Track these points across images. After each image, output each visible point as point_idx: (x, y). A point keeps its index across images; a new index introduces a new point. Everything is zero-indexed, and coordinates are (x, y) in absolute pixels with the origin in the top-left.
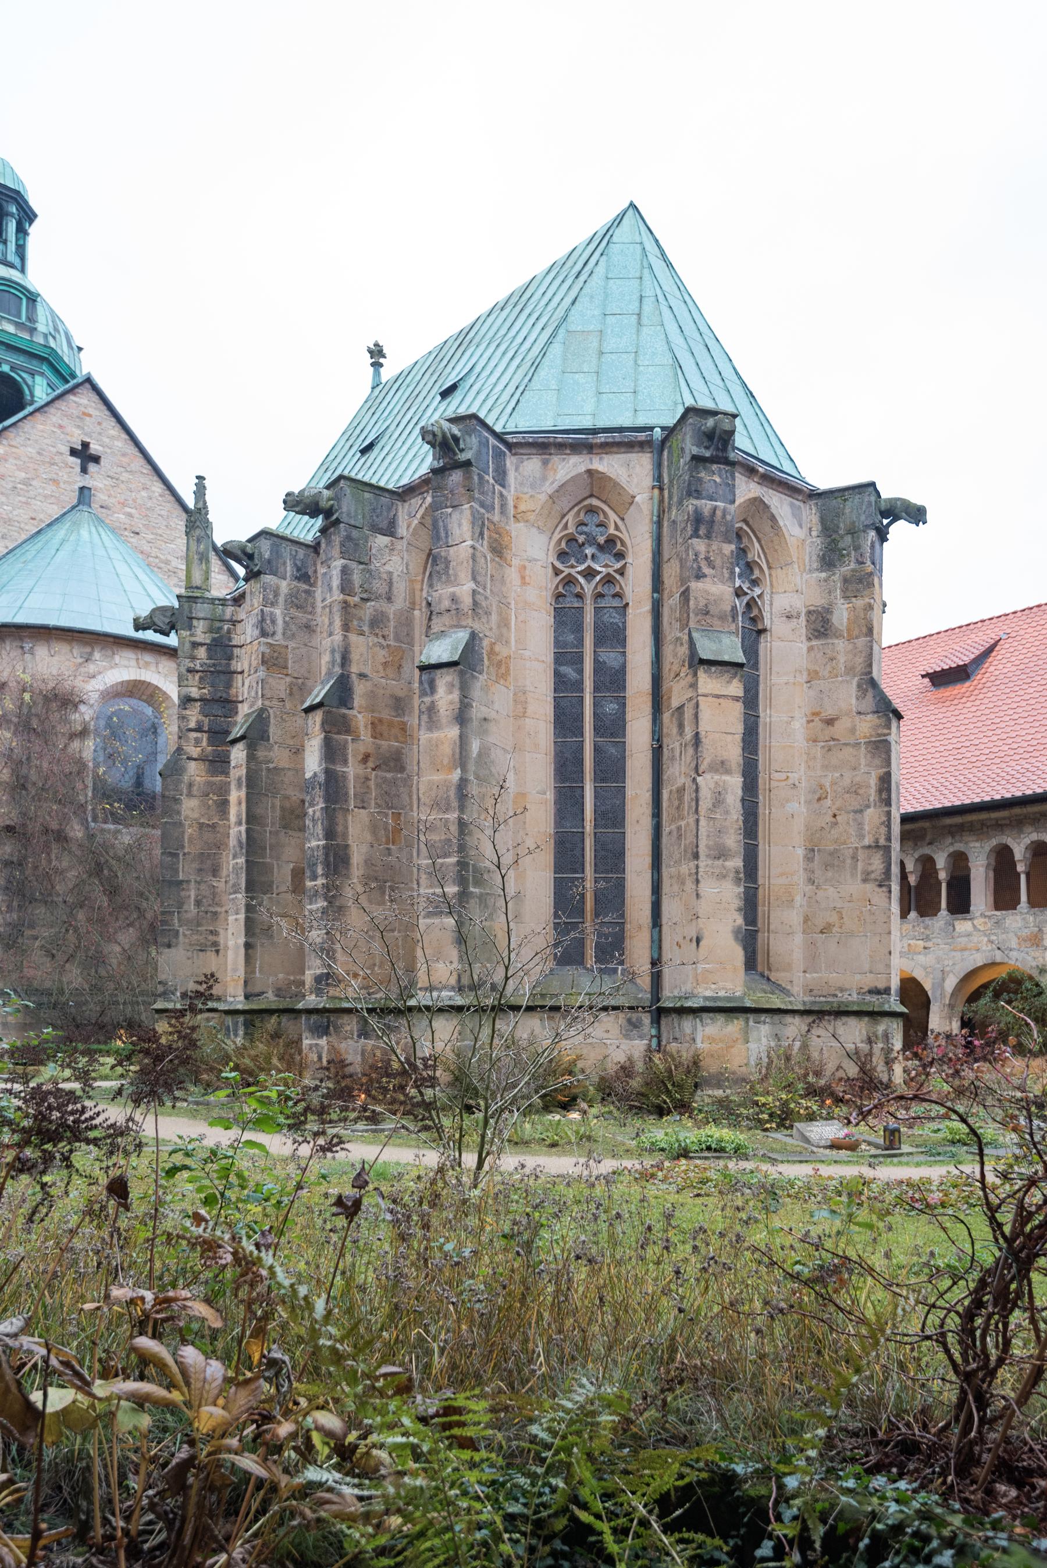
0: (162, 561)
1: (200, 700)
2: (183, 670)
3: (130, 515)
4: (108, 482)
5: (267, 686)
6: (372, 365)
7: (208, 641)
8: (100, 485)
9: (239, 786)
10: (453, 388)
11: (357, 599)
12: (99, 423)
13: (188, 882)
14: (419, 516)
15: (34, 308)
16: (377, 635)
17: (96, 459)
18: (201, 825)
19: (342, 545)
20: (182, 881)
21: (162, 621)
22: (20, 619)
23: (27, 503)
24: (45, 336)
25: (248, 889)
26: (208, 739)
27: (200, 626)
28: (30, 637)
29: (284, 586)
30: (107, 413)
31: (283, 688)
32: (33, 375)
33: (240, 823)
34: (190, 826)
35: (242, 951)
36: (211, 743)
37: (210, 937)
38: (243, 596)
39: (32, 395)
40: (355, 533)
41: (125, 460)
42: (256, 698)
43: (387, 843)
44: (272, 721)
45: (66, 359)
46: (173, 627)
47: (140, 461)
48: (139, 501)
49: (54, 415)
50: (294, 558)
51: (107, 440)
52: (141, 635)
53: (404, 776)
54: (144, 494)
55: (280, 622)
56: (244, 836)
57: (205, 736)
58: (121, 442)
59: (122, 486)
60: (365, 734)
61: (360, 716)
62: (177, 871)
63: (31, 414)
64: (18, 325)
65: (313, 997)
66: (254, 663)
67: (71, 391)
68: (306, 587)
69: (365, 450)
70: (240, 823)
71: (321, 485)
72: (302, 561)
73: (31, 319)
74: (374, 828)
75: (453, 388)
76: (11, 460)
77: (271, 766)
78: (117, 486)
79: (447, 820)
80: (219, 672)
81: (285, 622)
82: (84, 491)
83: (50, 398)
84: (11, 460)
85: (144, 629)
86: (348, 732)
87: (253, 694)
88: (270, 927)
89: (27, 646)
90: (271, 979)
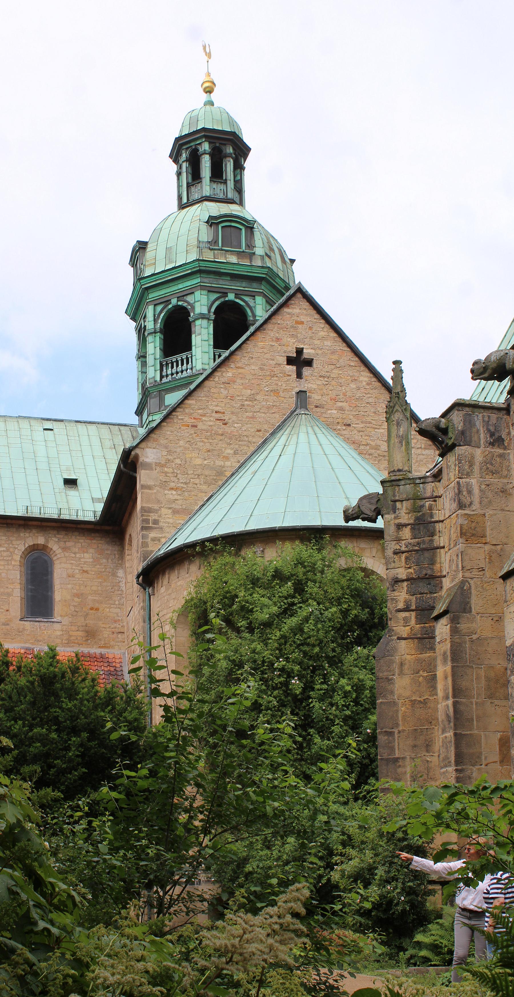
0: (372, 448)
1: (407, 580)
3: (341, 409)
4: (322, 381)
5: (466, 558)
7: (412, 521)
8: (314, 386)
12: (311, 328)
13: (404, 758)
15: (252, 233)
18: (413, 702)
21: (368, 509)
22: (253, 526)
23: (253, 417)
24: (262, 257)
25: (457, 763)
26: (416, 618)
27: (403, 508)
28: (262, 542)
29: (479, 454)
30: (317, 316)
33: (447, 698)
34: (403, 705)
36: (419, 620)
38: (440, 471)
39: (254, 316)
42: (457, 571)
44: (473, 591)
47: (349, 354)
48: (348, 394)
49: (272, 331)
50: (487, 423)
51: (317, 342)
52: (352, 524)
54: (353, 386)
55: (476, 491)
57: (413, 614)
59: (333, 383)
62: (392, 749)
63: (253, 334)
64: (240, 254)
66: (454, 536)
67: (285, 304)
68: (501, 451)
71: (509, 347)
72: (495, 426)
73: (250, 245)
76: (239, 381)
77: (474, 637)
81: (481, 490)
82: (301, 394)
83: (270, 313)
84: (239, 381)
85: (353, 519)
87: (454, 567)
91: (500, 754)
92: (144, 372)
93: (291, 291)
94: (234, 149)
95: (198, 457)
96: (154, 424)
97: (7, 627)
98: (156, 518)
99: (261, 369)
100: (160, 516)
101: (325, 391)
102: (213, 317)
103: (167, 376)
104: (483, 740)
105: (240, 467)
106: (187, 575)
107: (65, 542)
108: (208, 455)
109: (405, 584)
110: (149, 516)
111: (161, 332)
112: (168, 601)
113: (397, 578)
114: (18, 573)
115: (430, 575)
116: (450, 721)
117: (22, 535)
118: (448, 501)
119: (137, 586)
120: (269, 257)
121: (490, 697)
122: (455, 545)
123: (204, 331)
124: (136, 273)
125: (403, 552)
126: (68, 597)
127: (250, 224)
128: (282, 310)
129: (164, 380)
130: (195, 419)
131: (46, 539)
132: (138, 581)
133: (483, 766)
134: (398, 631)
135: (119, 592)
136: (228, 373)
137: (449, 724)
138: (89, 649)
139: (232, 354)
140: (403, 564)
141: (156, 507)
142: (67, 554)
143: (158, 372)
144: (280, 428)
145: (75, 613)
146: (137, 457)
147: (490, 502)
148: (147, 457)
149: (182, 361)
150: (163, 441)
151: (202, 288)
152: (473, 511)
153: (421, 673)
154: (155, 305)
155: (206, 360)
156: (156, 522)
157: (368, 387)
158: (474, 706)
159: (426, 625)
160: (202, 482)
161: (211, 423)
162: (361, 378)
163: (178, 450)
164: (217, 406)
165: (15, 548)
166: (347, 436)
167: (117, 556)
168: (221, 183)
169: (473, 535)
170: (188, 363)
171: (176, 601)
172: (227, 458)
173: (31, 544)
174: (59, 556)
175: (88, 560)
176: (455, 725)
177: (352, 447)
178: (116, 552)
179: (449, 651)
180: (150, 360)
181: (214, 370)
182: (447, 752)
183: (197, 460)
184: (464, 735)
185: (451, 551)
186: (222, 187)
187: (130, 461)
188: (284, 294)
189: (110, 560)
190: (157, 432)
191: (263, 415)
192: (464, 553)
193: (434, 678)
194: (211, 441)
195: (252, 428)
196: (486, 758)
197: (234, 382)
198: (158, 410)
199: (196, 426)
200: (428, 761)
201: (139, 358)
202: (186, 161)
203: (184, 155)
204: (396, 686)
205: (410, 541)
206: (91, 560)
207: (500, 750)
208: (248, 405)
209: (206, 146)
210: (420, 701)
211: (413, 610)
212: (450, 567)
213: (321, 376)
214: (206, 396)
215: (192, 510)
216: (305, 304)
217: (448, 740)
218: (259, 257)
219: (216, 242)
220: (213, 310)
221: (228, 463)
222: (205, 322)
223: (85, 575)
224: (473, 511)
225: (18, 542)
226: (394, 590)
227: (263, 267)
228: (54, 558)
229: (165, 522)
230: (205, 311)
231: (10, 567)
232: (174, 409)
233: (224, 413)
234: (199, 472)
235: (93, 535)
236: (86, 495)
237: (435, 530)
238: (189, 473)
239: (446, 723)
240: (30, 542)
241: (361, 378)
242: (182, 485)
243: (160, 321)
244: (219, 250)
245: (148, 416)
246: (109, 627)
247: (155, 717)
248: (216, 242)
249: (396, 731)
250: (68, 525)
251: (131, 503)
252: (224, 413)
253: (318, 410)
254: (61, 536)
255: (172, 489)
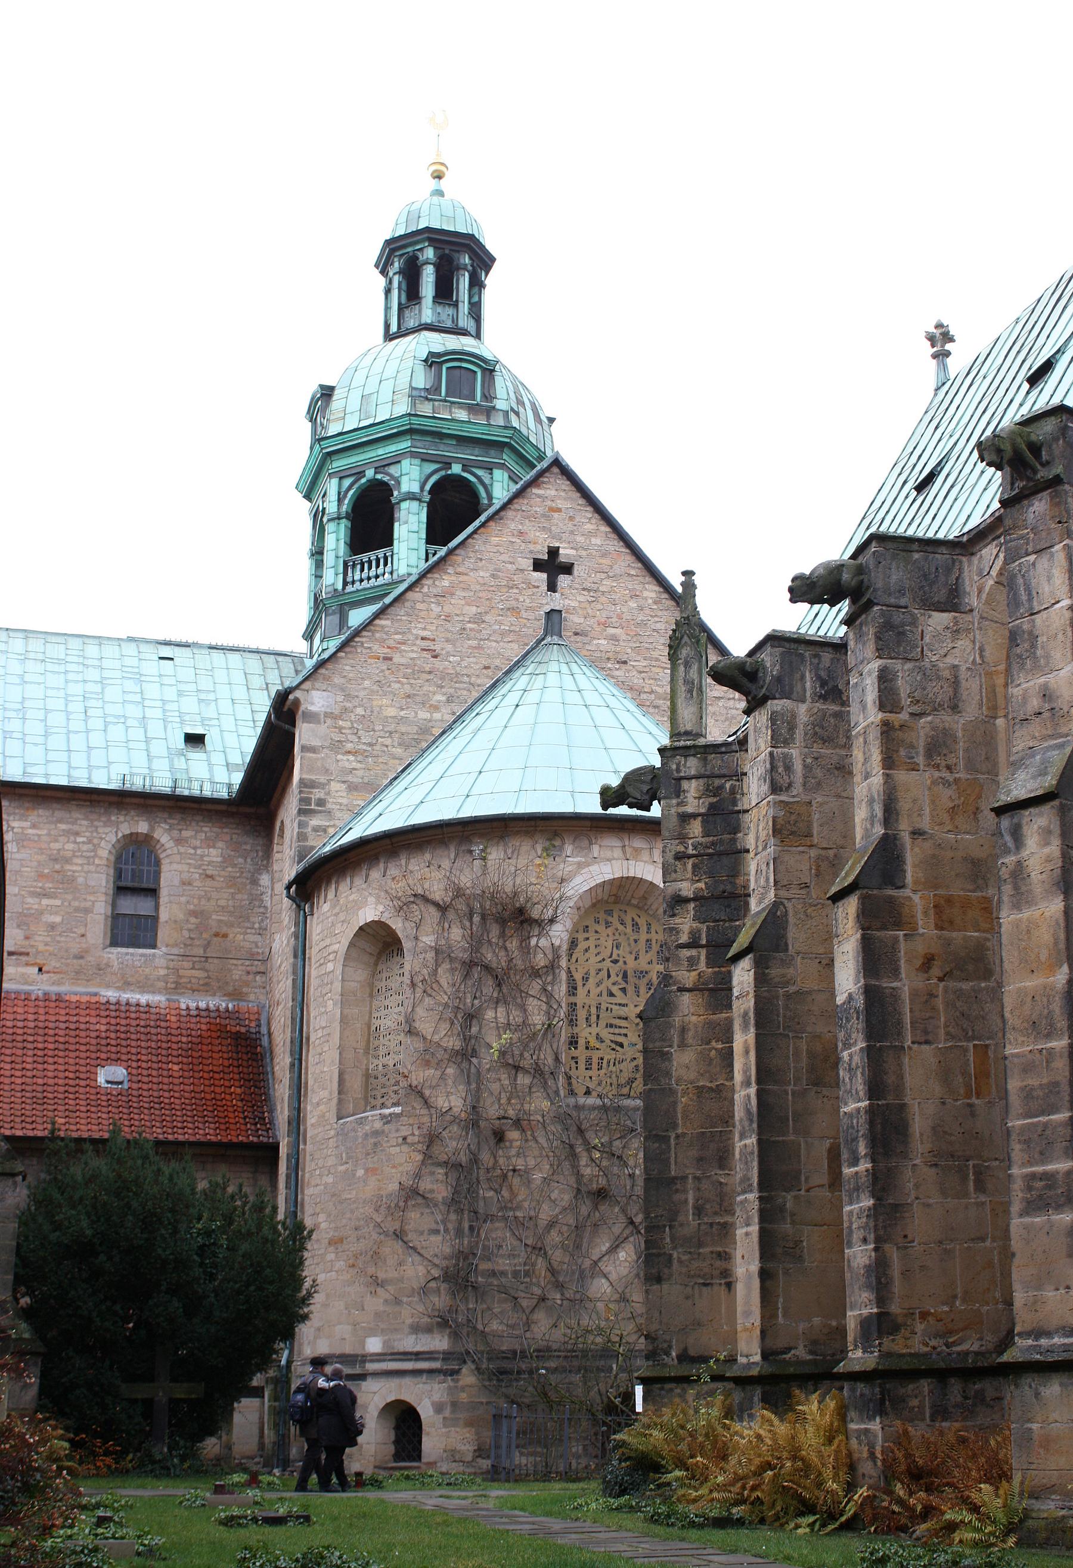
1: (694, 899)
2: (670, 856)
3: (614, 638)
5: (782, 868)
6: (935, 356)
7: (702, 810)
9: (745, 1027)
10: (1047, 367)
11: (904, 716)
12: (571, 518)
14: (994, 573)
16: (937, 767)
17: (568, 569)
18: (700, 1090)
19: (878, 638)
20: (676, 1178)
22: (469, 811)
24: (506, 413)
25: (763, 1185)
26: (707, 958)
27: (692, 788)
28: (482, 836)
29: (803, 711)
30: (582, 501)
31: (805, 867)
32: (490, 470)
34: (685, 1093)
35: (756, 1283)
37: (718, 1263)
39: (490, 497)
40: (897, 618)
41: (605, 561)
43: (968, 1096)
44: (791, 919)
45: (533, 440)
46: (653, 798)
49: (513, 521)
51: (580, 539)
53: (992, 984)
54: (633, 604)
55: (798, 767)
56: (754, 1102)
57: (703, 952)
58: (600, 538)
59: (603, 599)
60: (925, 927)
61: (916, 898)
63: (483, 525)
64: (472, 409)
65: (859, 1353)
66: (763, 835)
67: (534, 482)
69: (921, 487)
70: (747, 1083)
72: (829, 670)
73: (489, 396)
74: (945, 1075)
75: (1047, 367)
76: (460, 593)
77: (792, 989)
78: (596, 601)
79: (1051, 1051)
80: (720, 854)
81: (805, 766)
82: (553, 617)
84: (460, 593)
85: (615, 805)
86: (898, 925)
87: (762, 882)
88: (798, 1243)
89: (477, 849)
90: (802, 1326)
91: (829, 1174)
92: (318, 576)
93: (545, 464)
94: (470, 258)
95: (392, 706)
96: (326, 655)
97: (81, 961)
98: (322, 795)
99: (493, 576)
100: (328, 793)
101: (590, 611)
102: (427, 498)
103: (353, 582)
104: (803, 1152)
105: (454, 722)
106: (364, 886)
107: (180, 830)
108: (407, 703)
109: (692, 905)
110: (311, 793)
111: (347, 517)
112: (333, 925)
113: (679, 896)
114: (104, 877)
115: (730, 893)
116: (751, 1121)
117: (113, 818)
118: (755, 782)
119: (287, 902)
120: (517, 414)
121: (816, 1084)
122: (765, 848)
123: (413, 519)
124: (314, 431)
125: (689, 857)
126: (181, 916)
127: (490, 365)
128: (529, 490)
129: (349, 588)
130: (389, 647)
131: (150, 825)
132: (289, 892)
133: (802, 1192)
134: (680, 978)
135: (262, 910)
136: (444, 581)
137: (750, 1125)
138: (138, 996)
139: (451, 552)
140: (689, 875)
141: (322, 779)
142: (182, 850)
143: (341, 577)
144: (518, 664)
145: (189, 942)
146: (297, 703)
147: (819, 784)
148: (313, 704)
149: (378, 560)
150: (337, 680)
151: (413, 455)
152: (794, 796)
153: (714, 1044)
154: (341, 478)
155: (414, 562)
156: (321, 802)
157: (655, 607)
158: (790, 1097)
159: (723, 969)
160: (396, 744)
161: (414, 655)
162: (646, 594)
163: (362, 694)
164: (424, 629)
165: (102, 839)
166: (620, 679)
167: (260, 854)
168: (450, 305)
169: (793, 833)
170: (386, 564)
171: (345, 925)
172: (436, 708)
173: (128, 832)
174: (169, 852)
175: (215, 859)
176: (759, 1126)
177: (629, 695)
178: (259, 848)
179: (752, 1010)
180: (329, 558)
181: (423, 575)
182: (748, 1170)
183: (389, 709)
184: (774, 1142)
185: (758, 857)
186: (450, 311)
187: (286, 709)
188: (535, 466)
189: (249, 860)
190: (329, 666)
191: (494, 644)
192: (778, 861)
193: (730, 1053)
194: (412, 681)
195: (477, 663)
196: (807, 1179)
197: (452, 594)
198: (337, 632)
199: (390, 659)
200: (721, 1183)
201: (313, 555)
202: (399, 273)
203: (396, 265)
204: (675, 1063)
205: (700, 840)
206: (219, 859)
207: (829, 1166)
208: (471, 630)
209: (430, 253)
210: (711, 1088)
211: (702, 946)
212: (756, 881)
213: (584, 589)
214: (408, 615)
215: (379, 786)
216: (565, 484)
217: (749, 1150)
218: (501, 413)
219: (437, 389)
220: (428, 487)
221: (437, 716)
222: (415, 504)
223: (209, 882)
224: (794, 796)
225: (107, 830)
226: (674, 915)
227: (505, 427)
228: (162, 856)
229: (335, 803)
230: (415, 488)
231: (92, 868)
232: (357, 633)
233: (434, 640)
234: (392, 728)
235: (224, 820)
236: (218, 759)
237: (739, 825)
238: (377, 728)
239: (746, 1124)
240: (125, 829)
241: (646, 594)
242: (365, 747)
243: (346, 502)
244: (441, 401)
245: (322, 641)
246: (242, 965)
247: (305, 1108)
248: (437, 389)
249: (673, 1136)
250: (187, 804)
251: (285, 773)
252: (434, 640)
253: (579, 638)
254: (176, 822)
255: (349, 752)
